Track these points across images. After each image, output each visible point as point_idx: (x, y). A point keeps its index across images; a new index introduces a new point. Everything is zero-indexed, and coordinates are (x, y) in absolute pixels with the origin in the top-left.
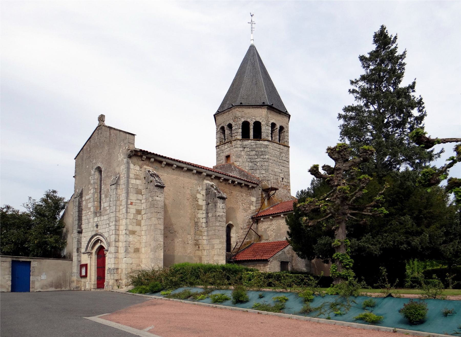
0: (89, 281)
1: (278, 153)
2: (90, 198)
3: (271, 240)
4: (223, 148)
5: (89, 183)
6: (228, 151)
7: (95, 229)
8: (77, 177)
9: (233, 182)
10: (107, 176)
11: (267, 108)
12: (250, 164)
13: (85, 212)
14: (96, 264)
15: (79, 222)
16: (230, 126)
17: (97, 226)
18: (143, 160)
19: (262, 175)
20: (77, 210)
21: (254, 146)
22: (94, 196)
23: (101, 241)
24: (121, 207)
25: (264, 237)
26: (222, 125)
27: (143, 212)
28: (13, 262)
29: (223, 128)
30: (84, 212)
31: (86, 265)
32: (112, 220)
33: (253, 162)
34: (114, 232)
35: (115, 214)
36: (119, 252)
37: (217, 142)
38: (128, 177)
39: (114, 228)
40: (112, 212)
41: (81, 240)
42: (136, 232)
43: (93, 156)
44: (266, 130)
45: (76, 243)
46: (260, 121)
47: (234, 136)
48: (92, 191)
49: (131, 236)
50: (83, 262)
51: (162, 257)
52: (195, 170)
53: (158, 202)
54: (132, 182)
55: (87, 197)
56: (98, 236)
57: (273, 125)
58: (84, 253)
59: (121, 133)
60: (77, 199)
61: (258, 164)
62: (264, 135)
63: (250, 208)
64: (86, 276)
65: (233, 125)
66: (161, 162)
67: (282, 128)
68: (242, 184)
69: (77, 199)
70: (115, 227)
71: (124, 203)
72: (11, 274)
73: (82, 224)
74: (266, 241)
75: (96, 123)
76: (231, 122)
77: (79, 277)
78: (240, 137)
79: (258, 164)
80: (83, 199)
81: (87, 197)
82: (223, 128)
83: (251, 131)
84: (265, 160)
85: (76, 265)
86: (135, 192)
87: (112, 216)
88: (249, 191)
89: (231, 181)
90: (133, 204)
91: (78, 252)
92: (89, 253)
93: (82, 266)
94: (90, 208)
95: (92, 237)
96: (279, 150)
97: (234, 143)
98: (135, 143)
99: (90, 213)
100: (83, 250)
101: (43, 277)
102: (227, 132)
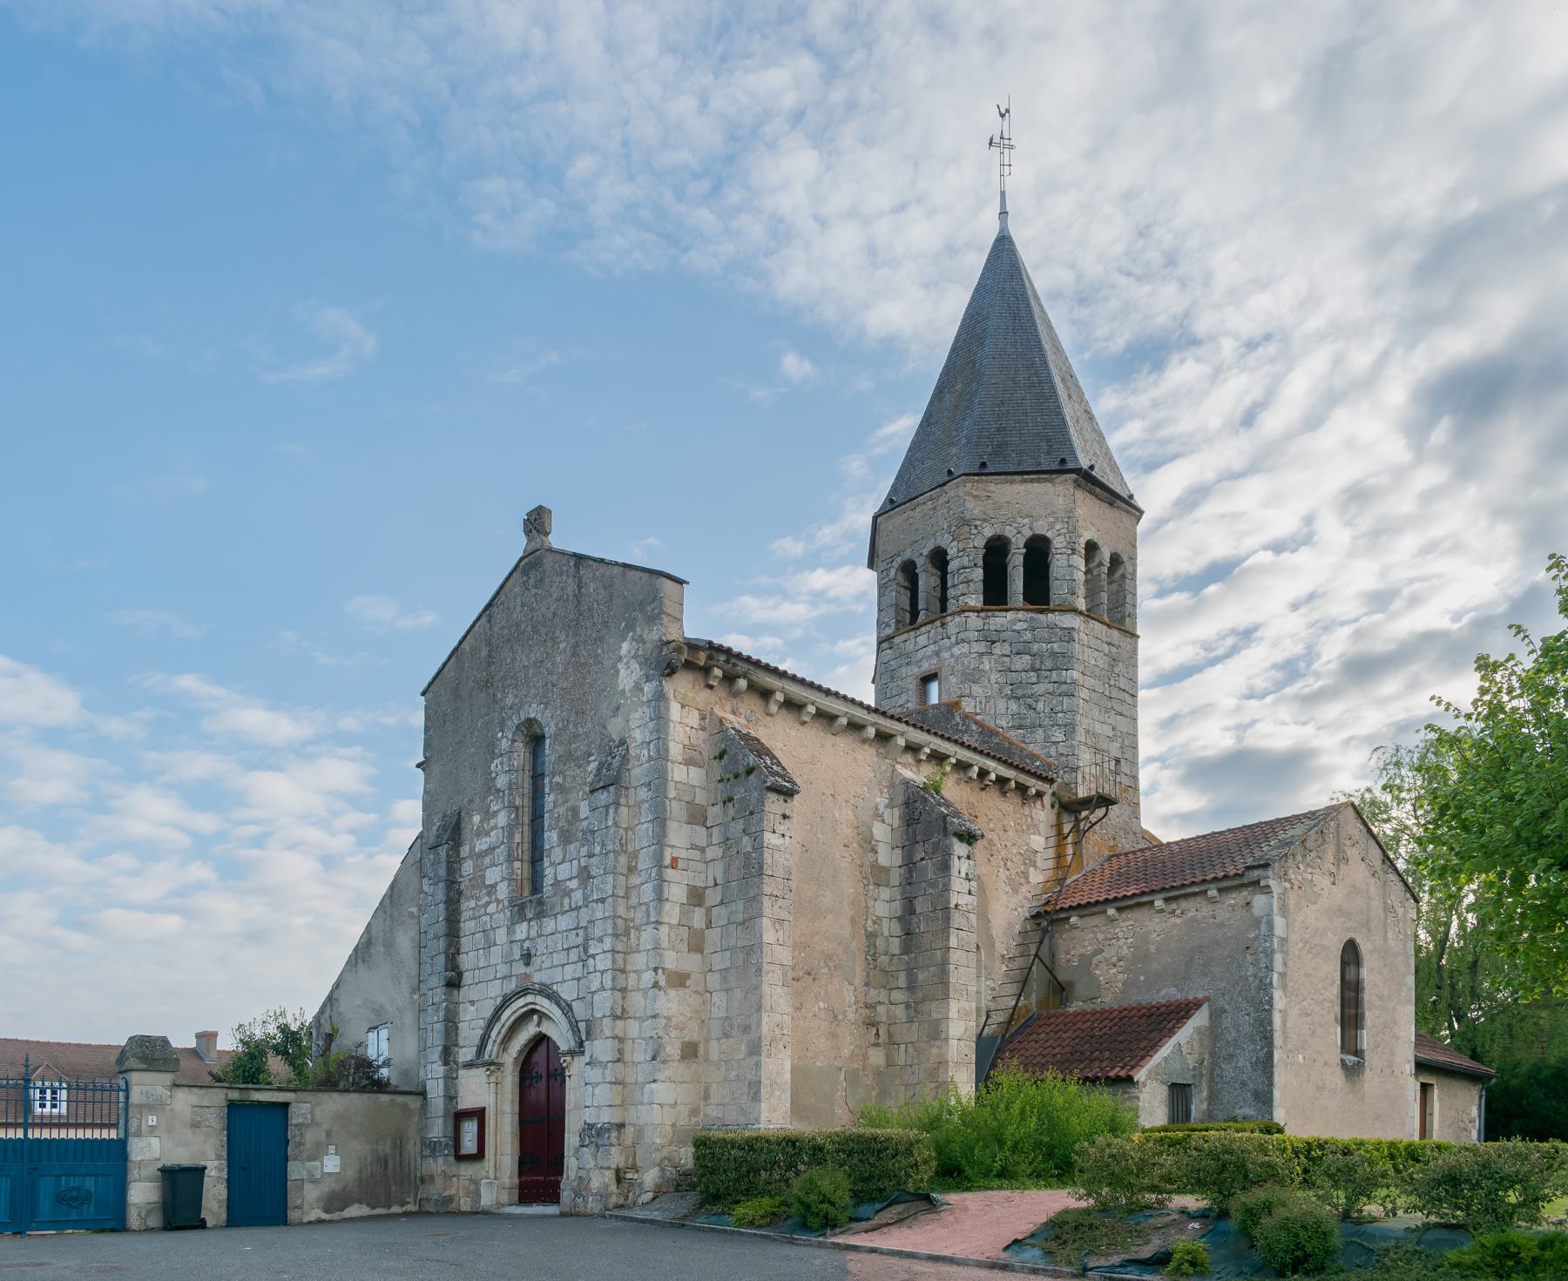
0: (491, 1175)
1: (1102, 662)
2: (492, 849)
3: (1108, 1000)
4: (910, 647)
5: (489, 787)
6: (930, 657)
7: (520, 968)
8: (436, 768)
9: (983, 773)
10: (568, 757)
11: (1075, 481)
12: (1014, 706)
13: (472, 903)
14: (517, 1108)
15: (449, 946)
16: (939, 559)
17: (527, 958)
18: (711, 687)
19: (1053, 749)
20: (441, 896)
21: (1028, 636)
22: (511, 836)
23: (543, 1016)
24: (635, 880)
25: (1081, 989)
26: (907, 555)
27: (712, 897)
28: (232, 1106)
29: (909, 569)
30: (467, 905)
31: (479, 1114)
32: (598, 932)
33: (1024, 696)
34: (608, 977)
35: (614, 908)
36: (627, 1057)
37: (880, 624)
38: (662, 755)
39: (609, 965)
40: (602, 900)
41: (456, 1014)
42: (688, 976)
43: (504, 678)
44: (1068, 569)
45: (439, 1027)
46: (1049, 535)
47: (956, 598)
48: (502, 819)
49: (672, 993)
50: (466, 1102)
51: (788, 1076)
52: (873, 724)
53: (777, 854)
54: (677, 778)
55: (481, 845)
56: (529, 998)
57: (1091, 548)
58: (470, 1065)
59: (631, 573)
60: (443, 851)
61: (1040, 706)
62: (1058, 591)
63: (1026, 875)
64: (480, 1155)
65: (951, 552)
66: (766, 694)
67: (1116, 561)
68: (1008, 780)
69: (443, 851)
70: (614, 961)
71: (644, 862)
72: (224, 1154)
73: (458, 952)
74: (1088, 1007)
75: (516, 545)
76: (944, 541)
77: (452, 1159)
78: (975, 600)
79: (1040, 706)
80: (462, 854)
81: (481, 845)
82: (909, 569)
83: (1020, 574)
84: (1064, 688)
85: (441, 1113)
86: (684, 816)
87: (599, 915)
88: (1027, 811)
89: (976, 769)
90: (681, 864)
91: (446, 1063)
92: (492, 1063)
93: (460, 1116)
94: (494, 886)
95: (507, 1001)
96: (1106, 648)
97: (954, 623)
98: (685, 617)
99: (492, 908)
100: (466, 1054)
101: (332, 1163)
102: (927, 581)
